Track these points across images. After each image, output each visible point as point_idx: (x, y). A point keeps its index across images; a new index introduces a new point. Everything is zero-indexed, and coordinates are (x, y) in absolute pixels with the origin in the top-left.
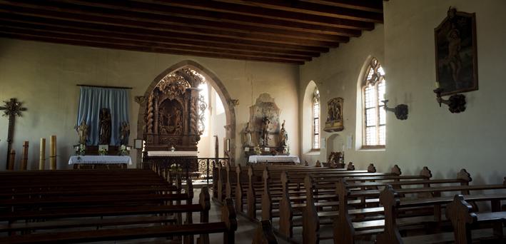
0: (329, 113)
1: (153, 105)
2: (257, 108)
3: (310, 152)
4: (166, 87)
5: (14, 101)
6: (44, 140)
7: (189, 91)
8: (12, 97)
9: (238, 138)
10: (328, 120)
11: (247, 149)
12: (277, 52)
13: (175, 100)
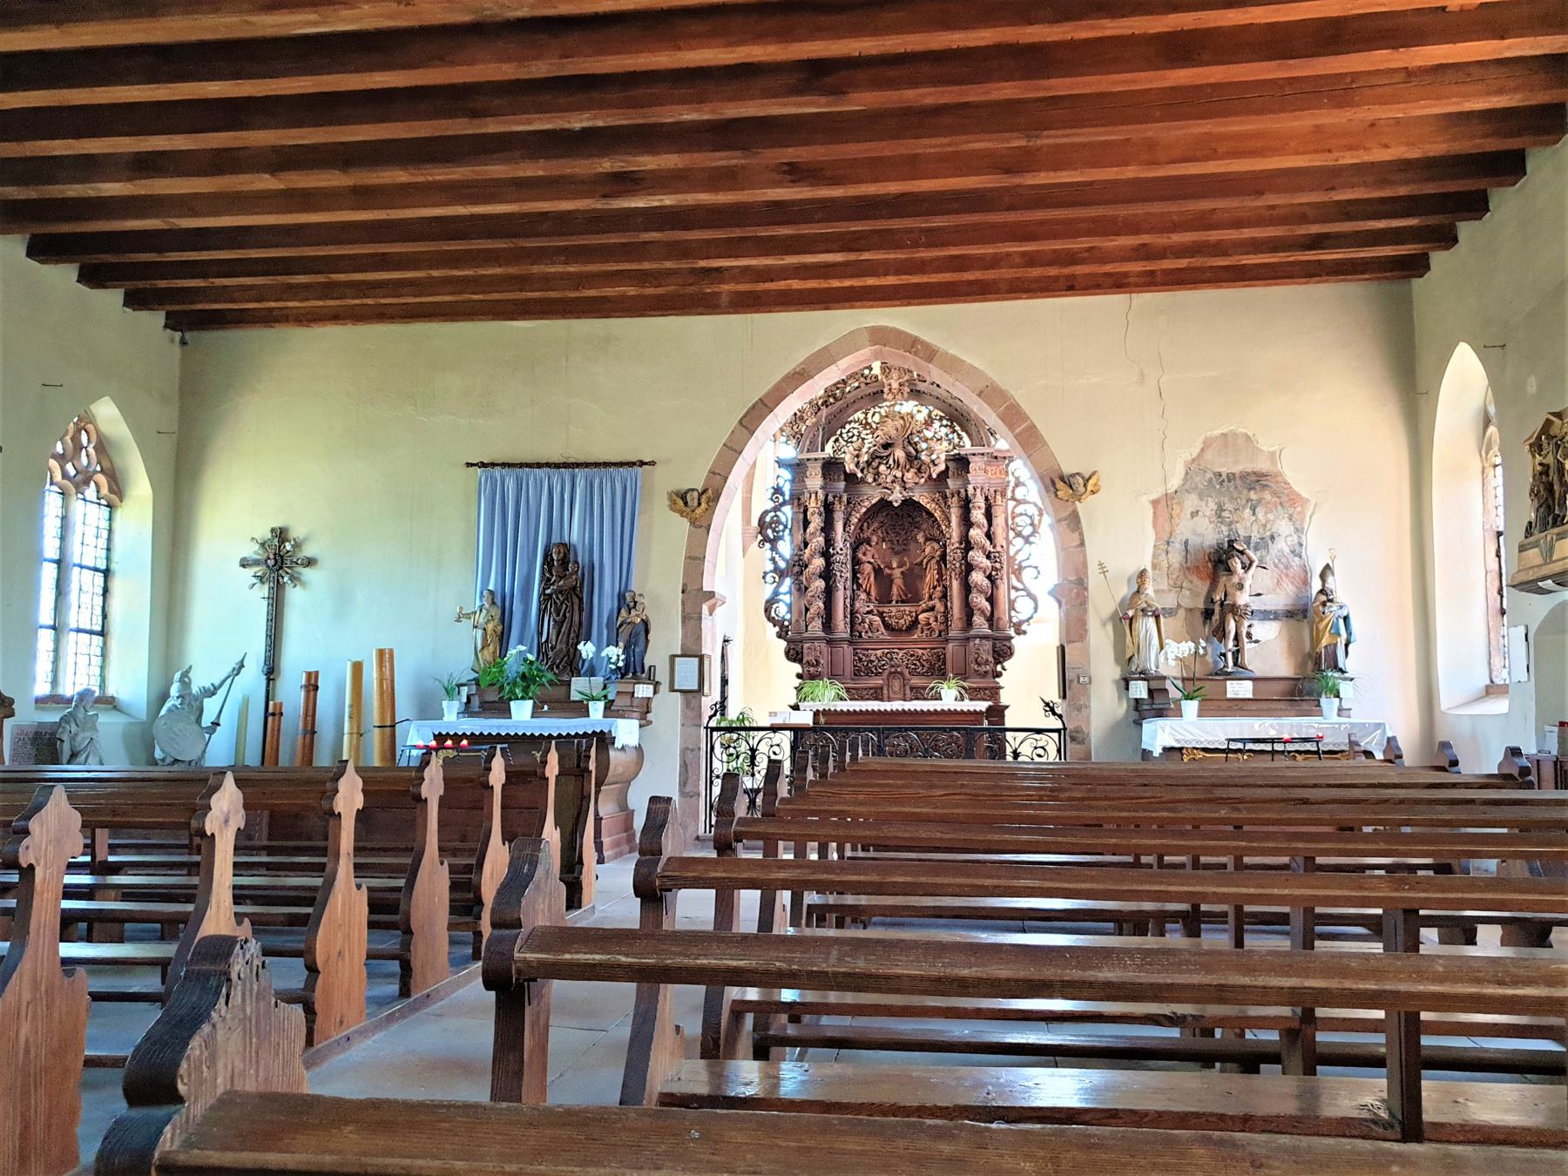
0: (1534, 493)
1: (828, 528)
2: (1191, 501)
3: (1478, 699)
4: (874, 457)
5: (281, 534)
6: (357, 668)
7: (961, 463)
8: (277, 525)
9: (1100, 639)
10: (1529, 531)
11: (1139, 690)
12: (1238, 224)
13: (910, 504)
